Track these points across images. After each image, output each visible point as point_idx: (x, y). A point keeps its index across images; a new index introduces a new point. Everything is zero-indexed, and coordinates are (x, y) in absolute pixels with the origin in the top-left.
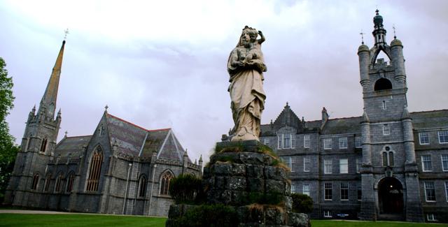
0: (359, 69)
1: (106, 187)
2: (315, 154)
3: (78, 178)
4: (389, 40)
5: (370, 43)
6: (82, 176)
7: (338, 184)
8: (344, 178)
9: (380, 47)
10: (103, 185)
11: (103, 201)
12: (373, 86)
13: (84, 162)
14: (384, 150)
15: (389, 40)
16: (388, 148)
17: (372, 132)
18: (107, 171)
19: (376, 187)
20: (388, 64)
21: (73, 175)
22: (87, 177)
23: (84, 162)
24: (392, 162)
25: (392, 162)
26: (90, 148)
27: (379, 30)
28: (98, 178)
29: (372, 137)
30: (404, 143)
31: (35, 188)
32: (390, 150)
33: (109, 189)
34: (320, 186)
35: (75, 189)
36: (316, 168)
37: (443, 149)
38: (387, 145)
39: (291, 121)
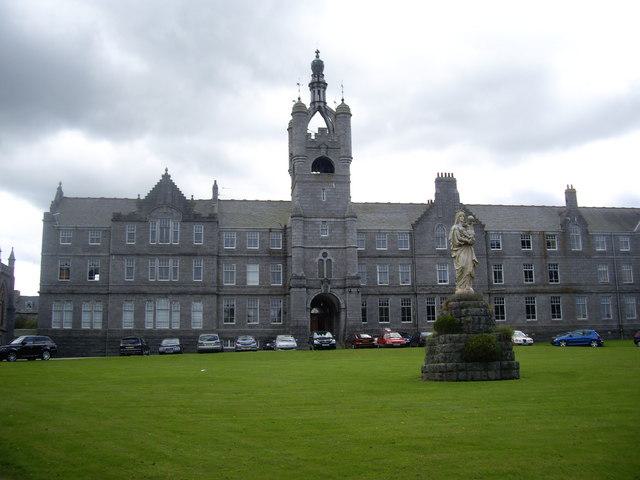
16: (325, 255)
20: (313, 137)
24: (329, 273)
25: (329, 273)
27: (318, 85)
38: (325, 251)
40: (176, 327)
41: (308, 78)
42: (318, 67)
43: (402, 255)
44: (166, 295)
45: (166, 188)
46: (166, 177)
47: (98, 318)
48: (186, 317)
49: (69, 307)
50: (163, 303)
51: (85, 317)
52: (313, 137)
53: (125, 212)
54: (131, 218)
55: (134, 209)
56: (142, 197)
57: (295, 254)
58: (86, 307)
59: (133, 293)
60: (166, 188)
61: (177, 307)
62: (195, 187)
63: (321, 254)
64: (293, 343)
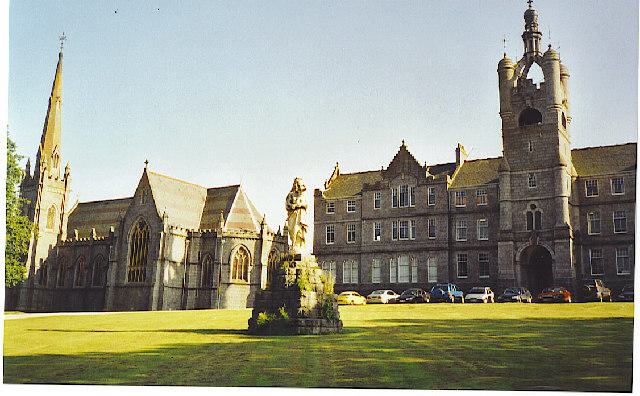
0: (217, 187)
1: (157, 278)
2: (443, 214)
3: (115, 264)
4: (543, 49)
5: (516, 52)
6: (120, 261)
7: (475, 255)
8: (483, 247)
9: (529, 59)
10: (153, 273)
11: (155, 295)
12: (517, 118)
13: (121, 243)
14: (529, 209)
15: (543, 49)
16: (533, 207)
17: (512, 185)
18: (156, 253)
19: (517, 259)
20: (538, 87)
21: (102, 269)
22: (128, 264)
23: (121, 243)
24: (538, 226)
25: (538, 226)
26: (129, 221)
27: (530, 36)
28: (144, 261)
29: (512, 191)
30: (554, 198)
31: (45, 282)
32: (537, 210)
33: (162, 277)
34: (450, 258)
35: (112, 280)
36: (443, 234)
37: (616, 203)
38: (533, 202)
39: (409, 168)
40: (414, 281)
41: (521, 27)
42: (529, 17)
43: (482, 211)
44: (405, 252)
45: (403, 158)
46: (403, 148)
47: (355, 274)
48: (422, 273)
49: (377, 262)
50: (403, 260)
51: (345, 274)
52: (538, 87)
53: (372, 182)
54: (377, 187)
55: (379, 178)
56: (385, 169)
57: (506, 207)
58: (345, 266)
59: (380, 252)
60: (403, 158)
61: (333, 265)
62: (428, 155)
63: (529, 207)
64: (264, 286)
